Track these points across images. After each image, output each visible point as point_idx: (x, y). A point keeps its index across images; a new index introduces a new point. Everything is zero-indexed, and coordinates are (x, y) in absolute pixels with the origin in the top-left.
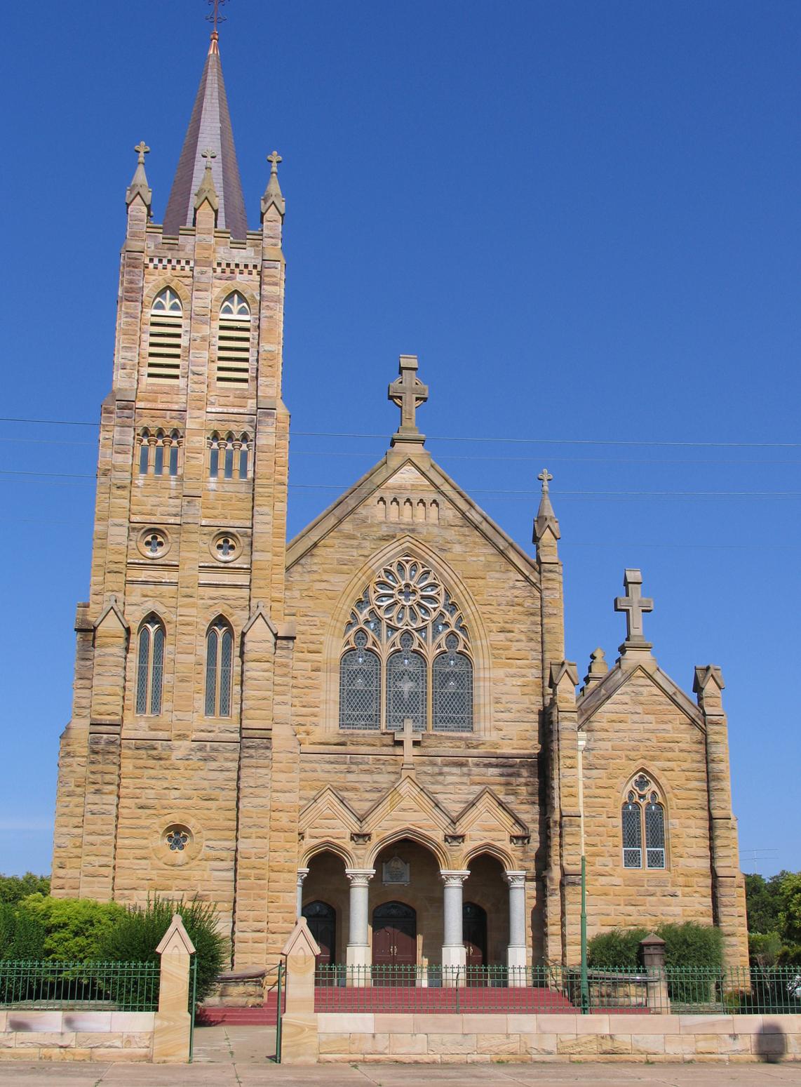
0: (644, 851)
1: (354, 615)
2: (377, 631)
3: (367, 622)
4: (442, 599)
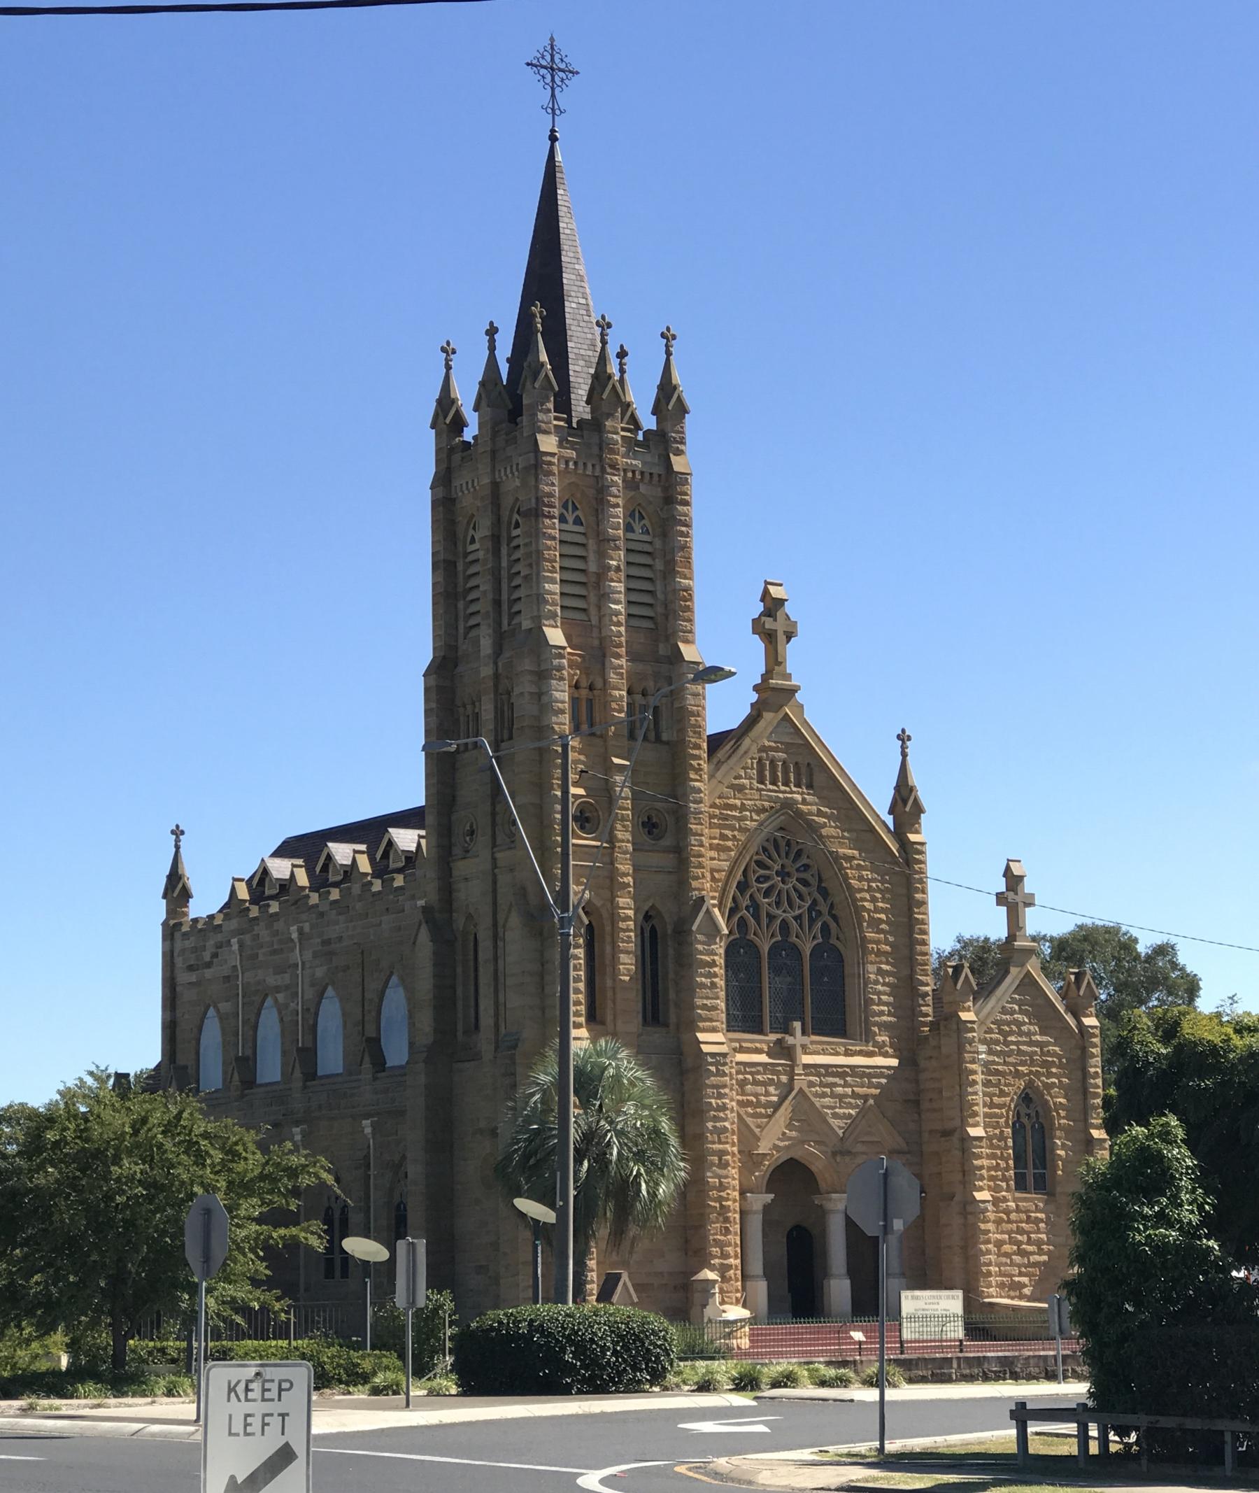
0: (1030, 1172)
3: (747, 908)
4: (814, 882)
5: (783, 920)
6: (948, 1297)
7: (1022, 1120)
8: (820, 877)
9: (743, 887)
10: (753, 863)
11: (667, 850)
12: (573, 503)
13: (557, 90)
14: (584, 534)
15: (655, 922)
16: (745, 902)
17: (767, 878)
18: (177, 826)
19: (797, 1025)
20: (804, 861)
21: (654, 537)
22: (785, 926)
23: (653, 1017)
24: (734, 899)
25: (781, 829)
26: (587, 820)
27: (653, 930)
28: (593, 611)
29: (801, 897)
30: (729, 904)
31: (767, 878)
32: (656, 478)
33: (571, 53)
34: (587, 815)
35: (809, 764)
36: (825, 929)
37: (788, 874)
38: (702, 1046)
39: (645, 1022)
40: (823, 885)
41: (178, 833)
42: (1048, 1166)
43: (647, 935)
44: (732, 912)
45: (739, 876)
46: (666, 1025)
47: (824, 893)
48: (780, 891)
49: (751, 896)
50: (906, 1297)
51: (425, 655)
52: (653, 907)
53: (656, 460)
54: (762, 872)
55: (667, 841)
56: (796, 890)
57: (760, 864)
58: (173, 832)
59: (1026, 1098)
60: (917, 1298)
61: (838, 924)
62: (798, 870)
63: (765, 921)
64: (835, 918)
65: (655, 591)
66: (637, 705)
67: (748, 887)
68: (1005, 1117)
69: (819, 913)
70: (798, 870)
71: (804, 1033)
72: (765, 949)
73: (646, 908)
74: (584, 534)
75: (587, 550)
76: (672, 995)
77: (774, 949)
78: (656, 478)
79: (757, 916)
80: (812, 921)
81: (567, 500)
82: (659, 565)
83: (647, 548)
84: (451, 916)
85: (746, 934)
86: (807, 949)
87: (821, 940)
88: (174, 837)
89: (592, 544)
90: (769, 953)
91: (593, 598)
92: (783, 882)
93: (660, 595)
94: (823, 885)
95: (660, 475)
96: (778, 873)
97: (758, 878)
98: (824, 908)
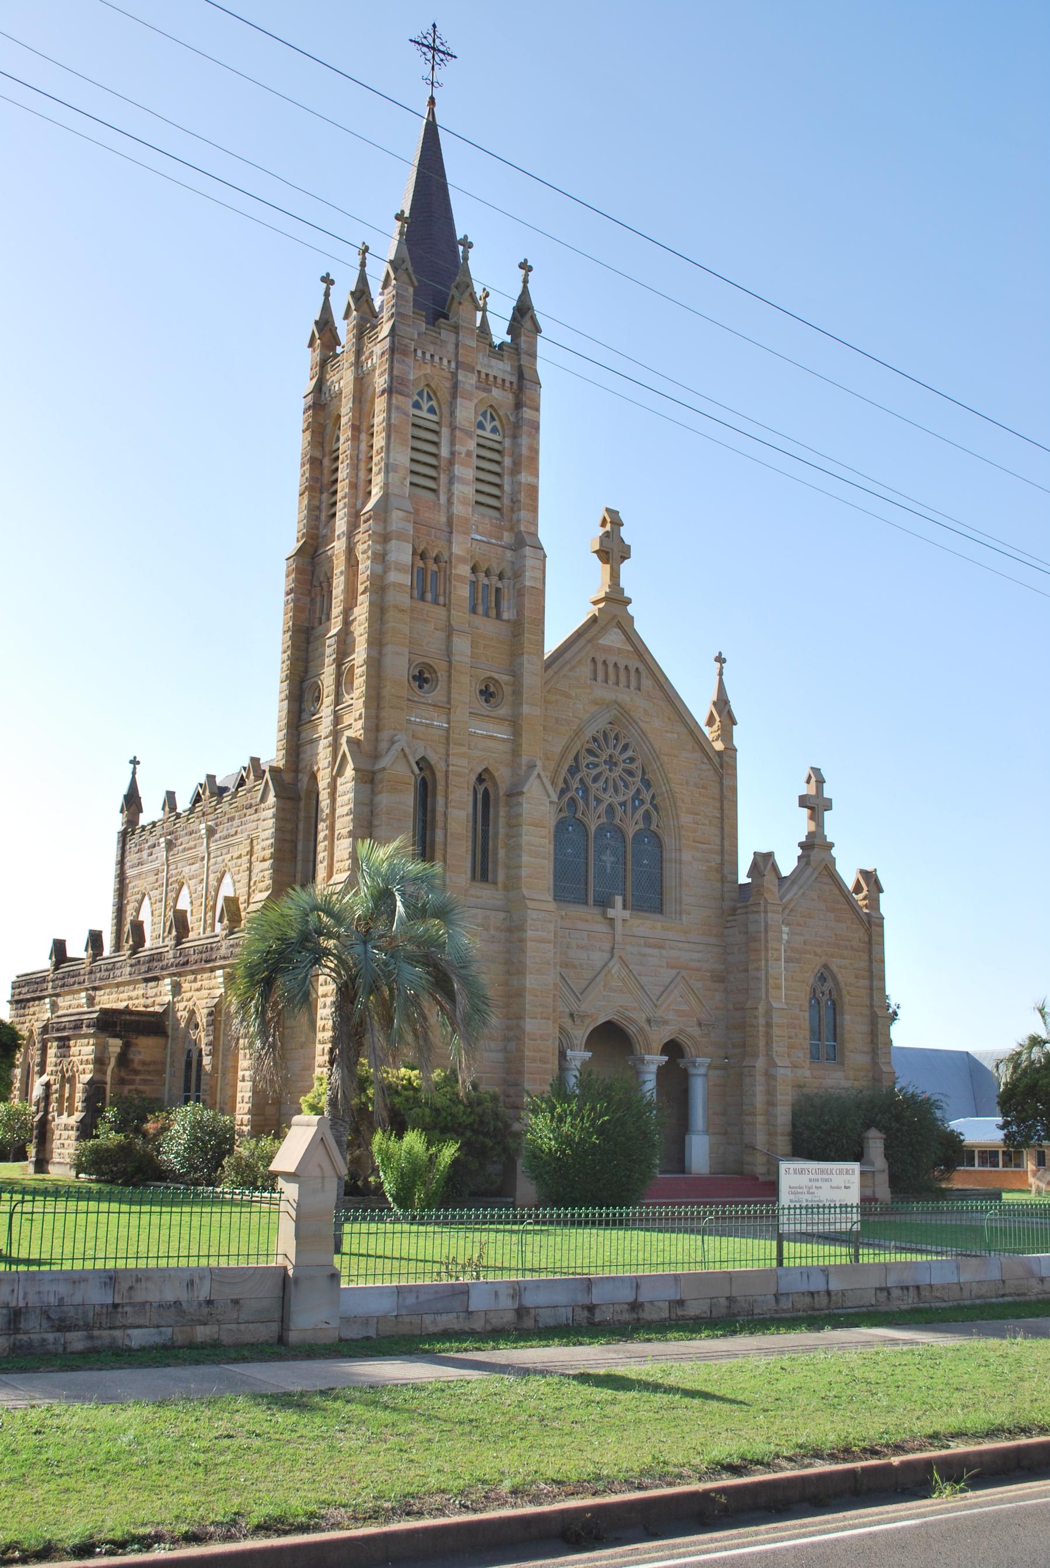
1: (565, 781)
2: (585, 797)
5: (610, 805)
6: (841, 1172)
7: (817, 996)
8: (643, 770)
9: (574, 770)
10: (584, 751)
11: (502, 719)
12: (428, 393)
13: (436, 67)
14: (437, 423)
15: (488, 784)
16: (575, 784)
17: (596, 765)
18: (135, 758)
19: (619, 900)
20: (629, 753)
21: (504, 437)
22: (611, 810)
23: (482, 876)
24: (565, 779)
25: (610, 723)
26: (426, 680)
27: (486, 793)
28: (442, 491)
29: (626, 786)
30: (561, 785)
31: (596, 765)
32: (507, 384)
33: (449, 39)
34: (426, 675)
35: (637, 669)
36: (647, 816)
37: (615, 764)
38: (527, 901)
39: (474, 878)
40: (646, 777)
41: (135, 762)
42: (838, 1039)
43: (480, 797)
44: (563, 792)
45: (570, 761)
46: (495, 883)
47: (648, 784)
48: (607, 778)
49: (581, 780)
50: (787, 1171)
51: (292, 545)
52: (486, 770)
53: (509, 369)
54: (592, 759)
55: (503, 711)
56: (622, 779)
57: (590, 752)
58: (131, 762)
59: (824, 975)
60: (801, 1172)
61: (658, 813)
62: (624, 761)
63: (593, 803)
64: (655, 807)
65: (503, 462)
66: (480, 583)
67: (579, 771)
68: (803, 995)
69: (642, 802)
70: (624, 761)
71: (625, 907)
72: (593, 828)
73: (479, 770)
74: (437, 423)
75: (440, 437)
76: (501, 853)
77: (600, 829)
78: (507, 384)
79: (585, 797)
80: (635, 809)
81: (423, 390)
82: (507, 461)
83: (496, 446)
84: (297, 777)
85: (575, 814)
86: (630, 832)
87: (642, 826)
88: (132, 766)
89: (445, 431)
90: (596, 833)
91: (443, 478)
92: (611, 770)
93: (507, 488)
94: (646, 777)
95: (511, 383)
96: (605, 762)
97: (588, 765)
98: (646, 796)
